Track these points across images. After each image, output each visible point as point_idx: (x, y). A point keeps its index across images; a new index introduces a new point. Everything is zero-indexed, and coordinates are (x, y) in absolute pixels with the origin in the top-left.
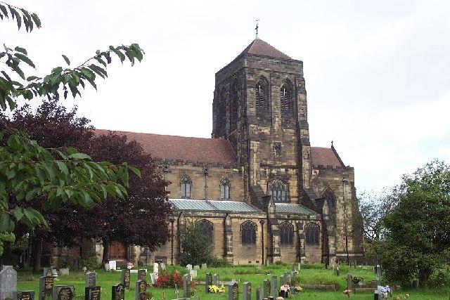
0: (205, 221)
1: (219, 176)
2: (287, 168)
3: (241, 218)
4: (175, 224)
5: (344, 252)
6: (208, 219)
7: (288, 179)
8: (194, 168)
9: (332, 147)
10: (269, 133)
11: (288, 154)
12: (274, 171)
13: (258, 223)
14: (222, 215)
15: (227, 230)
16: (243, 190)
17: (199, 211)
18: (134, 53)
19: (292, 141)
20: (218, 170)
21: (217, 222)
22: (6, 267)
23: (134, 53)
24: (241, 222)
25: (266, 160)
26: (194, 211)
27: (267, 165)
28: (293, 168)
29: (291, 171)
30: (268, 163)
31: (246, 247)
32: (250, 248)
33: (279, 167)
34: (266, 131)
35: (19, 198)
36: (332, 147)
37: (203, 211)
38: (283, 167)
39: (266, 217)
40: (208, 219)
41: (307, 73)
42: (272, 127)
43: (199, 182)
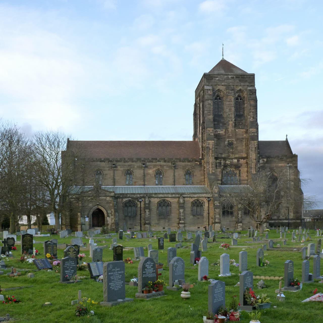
0: (164, 200)
1: (184, 168)
2: (238, 159)
3: (192, 198)
4: (142, 203)
5: (286, 219)
6: (166, 199)
7: (239, 167)
8: (165, 164)
9: (287, 139)
10: (224, 134)
11: (239, 148)
12: (228, 162)
13: (205, 201)
14: (177, 195)
15: (182, 206)
16: (203, 177)
17: (160, 194)
18: (287, 136)
19: (243, 139)
20: (183, 164)
21: (174, 201)
22: (251, 322)
23: (287, 136)
24: (192, 200)
25: (222, 154)
26: (156, 194)
27: (222, 158)
28: (244, 158)
29: (242, 161)
30: (223, 156)
31: (195, 218)
32: (198, 218)
33: (232, 159)
34: (221, 132)
35: (69, 206)
36: (287, 139)
37: (163, 194)
38: (235, 158)
39: (211, 196)
40: (166, 199)
41: (259, 85)
42: (227, 129)
43: (169, 174)
